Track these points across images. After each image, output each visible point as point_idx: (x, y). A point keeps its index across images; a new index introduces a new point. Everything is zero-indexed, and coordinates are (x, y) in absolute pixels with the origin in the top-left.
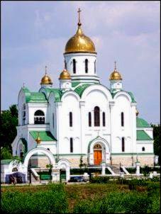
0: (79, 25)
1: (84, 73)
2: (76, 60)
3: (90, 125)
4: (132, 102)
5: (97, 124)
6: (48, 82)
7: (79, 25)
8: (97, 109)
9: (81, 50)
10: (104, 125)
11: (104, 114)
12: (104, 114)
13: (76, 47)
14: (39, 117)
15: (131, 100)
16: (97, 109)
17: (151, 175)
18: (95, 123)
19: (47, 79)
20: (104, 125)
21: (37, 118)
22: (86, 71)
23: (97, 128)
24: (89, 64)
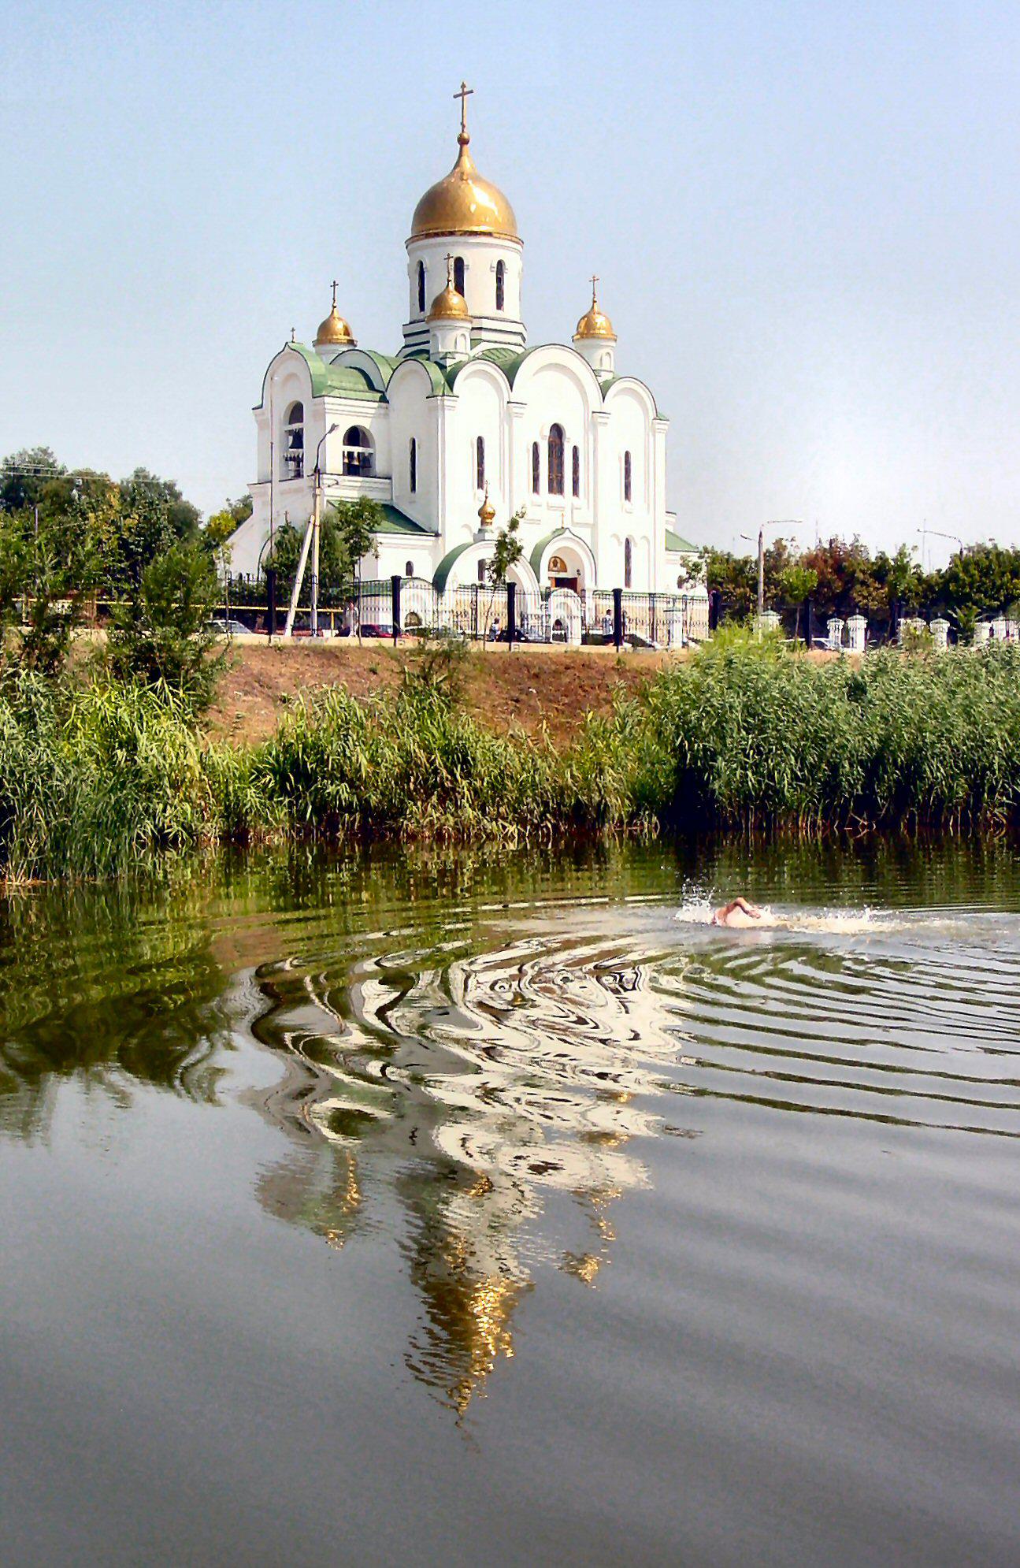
0: (463, 142)
1: (490, 308)
2: (507, 265)
3: (536, 489)
4: (658, 417)
5: (556, 486)
6: (345, 338)
7: (463, 142)
8: (557, 431)
9: (475, 229)
10: (575, 492)
11: (575, 449)
12: (575, 449)
13: (466, 217)
14: (356, 450)
15: (652, 414)
16: (557, 431)
17: (819, 822)
18: (551, 481)
19: (339, 326)
20: (575, 492)
21: (350, 455)
22: (500, 304)
23: (556, 499)
24: (506, 278)
